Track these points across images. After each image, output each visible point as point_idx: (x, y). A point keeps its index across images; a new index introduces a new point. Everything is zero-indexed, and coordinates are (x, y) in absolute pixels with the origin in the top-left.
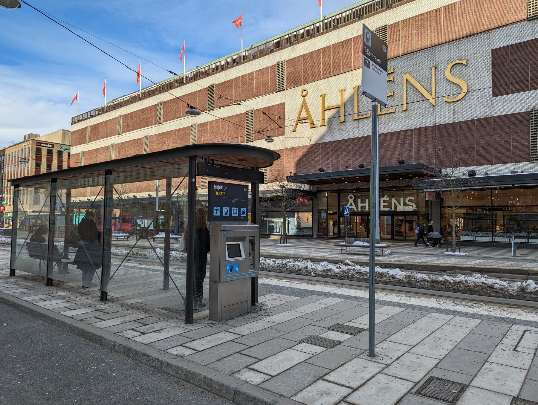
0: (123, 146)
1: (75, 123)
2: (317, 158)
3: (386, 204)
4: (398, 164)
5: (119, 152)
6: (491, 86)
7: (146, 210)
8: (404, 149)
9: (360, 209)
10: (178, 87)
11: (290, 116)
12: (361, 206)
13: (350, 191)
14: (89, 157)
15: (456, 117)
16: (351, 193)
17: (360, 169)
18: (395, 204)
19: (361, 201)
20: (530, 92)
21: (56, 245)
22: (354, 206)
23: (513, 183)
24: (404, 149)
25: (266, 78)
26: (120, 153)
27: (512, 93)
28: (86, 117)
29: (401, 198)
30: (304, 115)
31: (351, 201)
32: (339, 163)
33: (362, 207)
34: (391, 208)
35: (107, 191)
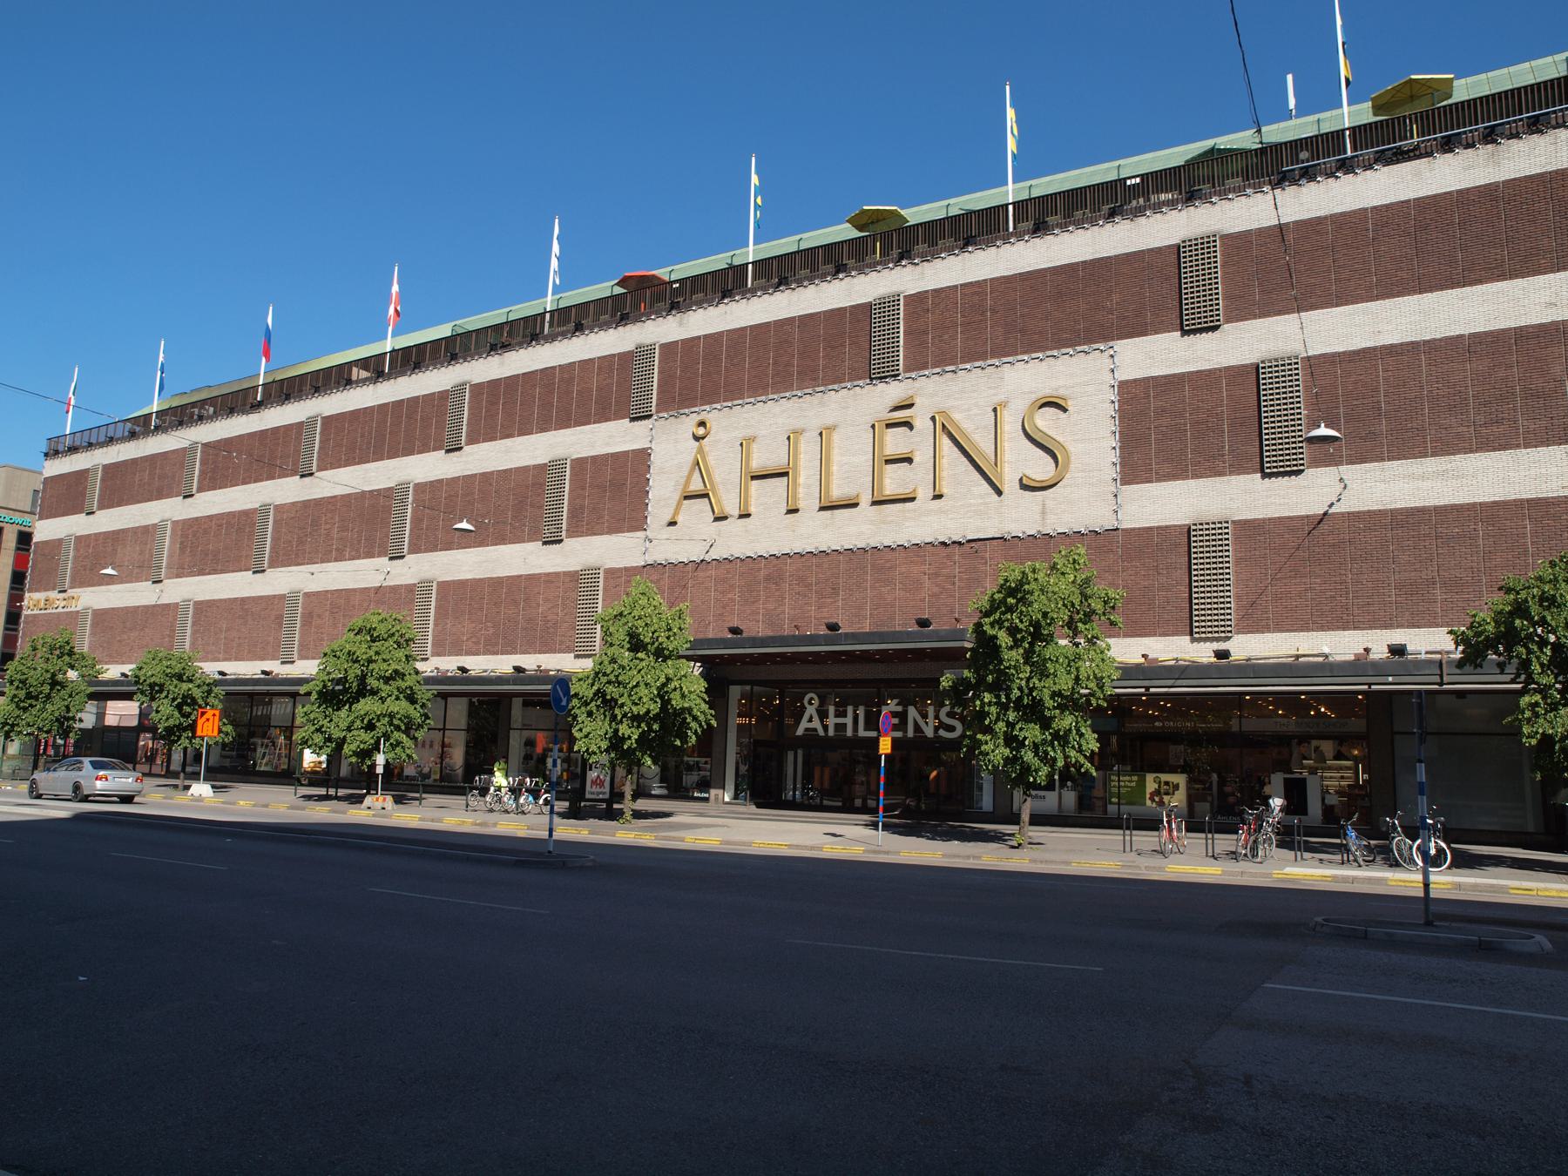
0: (195, 529)
1: (56, 453)
2: (730, 596)
3: (895, 721)
4: (916, 628)
5: (182, 543)
6: (1296, 315)
7: (179, 707)
8: (936, 590)
9: (831, 732)
10: (364, 382)
11: (662, 490)
12: (846, 716)
13: (812, 684)
14: (90, 551)
15: (1048, 521)
16: (811, 690)
17: (829, 632)
18: (915, 720)
19: (836, 711)
20: (1192, 483)
21: (557, 779)
22: (816, 724)
23: (1147, 683)
24: (936, 590)
25: (605, 382)
26: (186, 547)
27: (1158, 480)
28: (93, 440)
29: (789, 752)
30: (696, 485)
31: (811, 710)
32: (784, 612)
33: (844, 715)
34: (905, 731)
35: (524, 725)
